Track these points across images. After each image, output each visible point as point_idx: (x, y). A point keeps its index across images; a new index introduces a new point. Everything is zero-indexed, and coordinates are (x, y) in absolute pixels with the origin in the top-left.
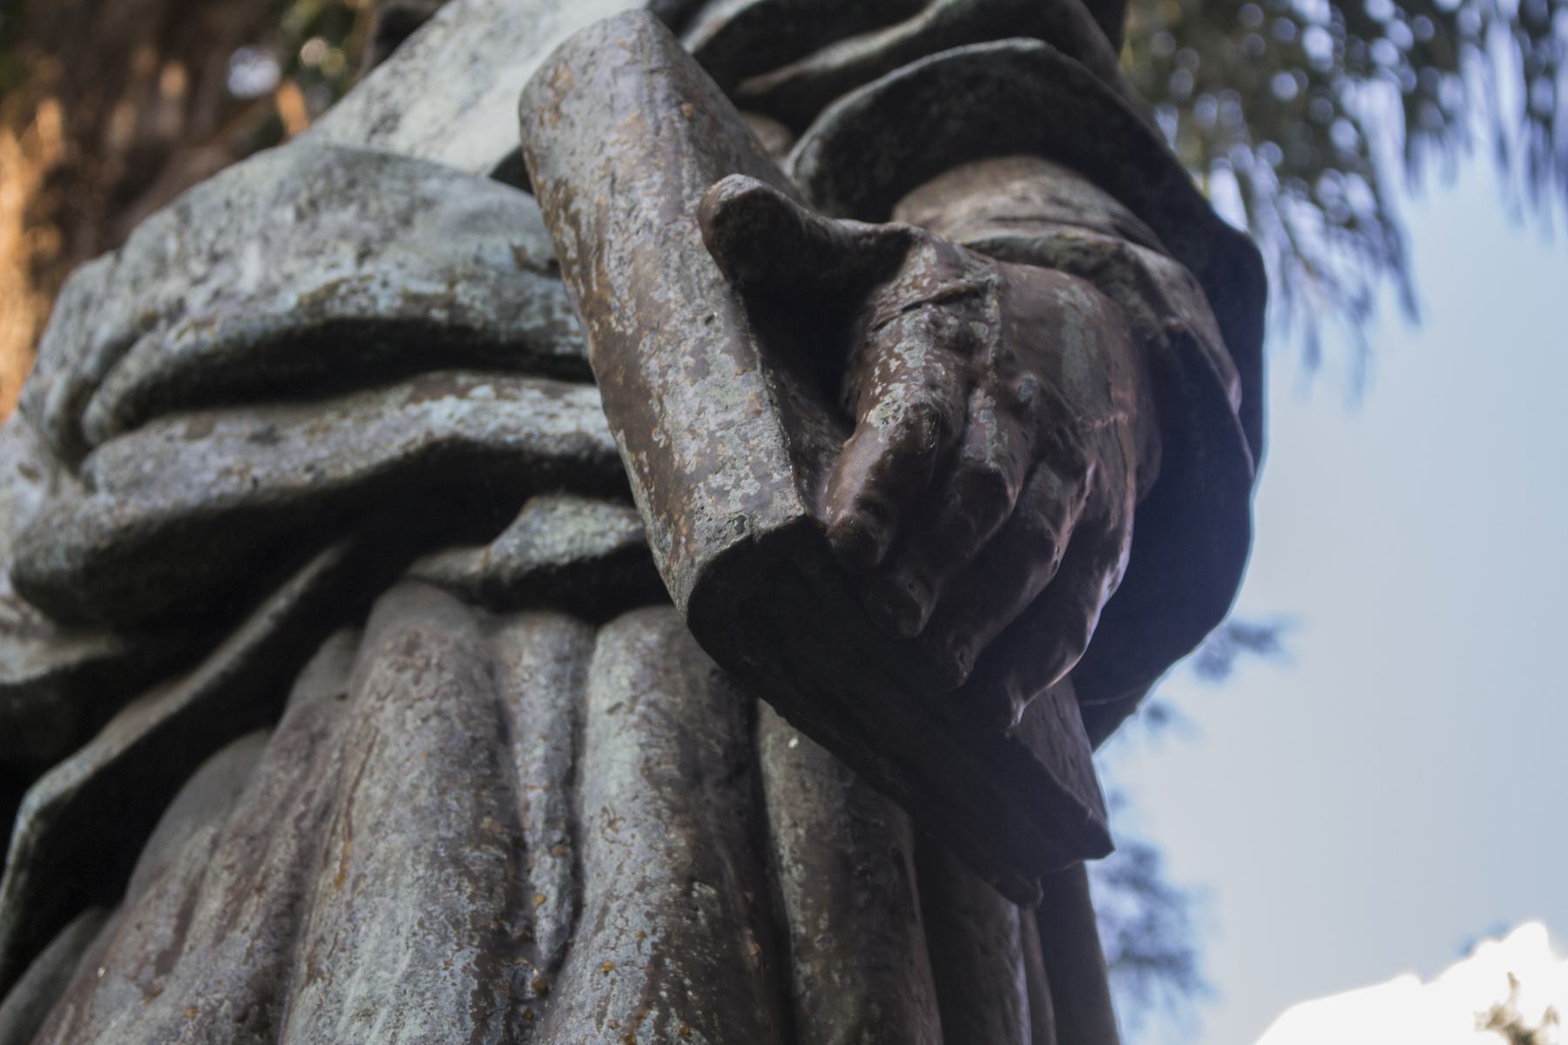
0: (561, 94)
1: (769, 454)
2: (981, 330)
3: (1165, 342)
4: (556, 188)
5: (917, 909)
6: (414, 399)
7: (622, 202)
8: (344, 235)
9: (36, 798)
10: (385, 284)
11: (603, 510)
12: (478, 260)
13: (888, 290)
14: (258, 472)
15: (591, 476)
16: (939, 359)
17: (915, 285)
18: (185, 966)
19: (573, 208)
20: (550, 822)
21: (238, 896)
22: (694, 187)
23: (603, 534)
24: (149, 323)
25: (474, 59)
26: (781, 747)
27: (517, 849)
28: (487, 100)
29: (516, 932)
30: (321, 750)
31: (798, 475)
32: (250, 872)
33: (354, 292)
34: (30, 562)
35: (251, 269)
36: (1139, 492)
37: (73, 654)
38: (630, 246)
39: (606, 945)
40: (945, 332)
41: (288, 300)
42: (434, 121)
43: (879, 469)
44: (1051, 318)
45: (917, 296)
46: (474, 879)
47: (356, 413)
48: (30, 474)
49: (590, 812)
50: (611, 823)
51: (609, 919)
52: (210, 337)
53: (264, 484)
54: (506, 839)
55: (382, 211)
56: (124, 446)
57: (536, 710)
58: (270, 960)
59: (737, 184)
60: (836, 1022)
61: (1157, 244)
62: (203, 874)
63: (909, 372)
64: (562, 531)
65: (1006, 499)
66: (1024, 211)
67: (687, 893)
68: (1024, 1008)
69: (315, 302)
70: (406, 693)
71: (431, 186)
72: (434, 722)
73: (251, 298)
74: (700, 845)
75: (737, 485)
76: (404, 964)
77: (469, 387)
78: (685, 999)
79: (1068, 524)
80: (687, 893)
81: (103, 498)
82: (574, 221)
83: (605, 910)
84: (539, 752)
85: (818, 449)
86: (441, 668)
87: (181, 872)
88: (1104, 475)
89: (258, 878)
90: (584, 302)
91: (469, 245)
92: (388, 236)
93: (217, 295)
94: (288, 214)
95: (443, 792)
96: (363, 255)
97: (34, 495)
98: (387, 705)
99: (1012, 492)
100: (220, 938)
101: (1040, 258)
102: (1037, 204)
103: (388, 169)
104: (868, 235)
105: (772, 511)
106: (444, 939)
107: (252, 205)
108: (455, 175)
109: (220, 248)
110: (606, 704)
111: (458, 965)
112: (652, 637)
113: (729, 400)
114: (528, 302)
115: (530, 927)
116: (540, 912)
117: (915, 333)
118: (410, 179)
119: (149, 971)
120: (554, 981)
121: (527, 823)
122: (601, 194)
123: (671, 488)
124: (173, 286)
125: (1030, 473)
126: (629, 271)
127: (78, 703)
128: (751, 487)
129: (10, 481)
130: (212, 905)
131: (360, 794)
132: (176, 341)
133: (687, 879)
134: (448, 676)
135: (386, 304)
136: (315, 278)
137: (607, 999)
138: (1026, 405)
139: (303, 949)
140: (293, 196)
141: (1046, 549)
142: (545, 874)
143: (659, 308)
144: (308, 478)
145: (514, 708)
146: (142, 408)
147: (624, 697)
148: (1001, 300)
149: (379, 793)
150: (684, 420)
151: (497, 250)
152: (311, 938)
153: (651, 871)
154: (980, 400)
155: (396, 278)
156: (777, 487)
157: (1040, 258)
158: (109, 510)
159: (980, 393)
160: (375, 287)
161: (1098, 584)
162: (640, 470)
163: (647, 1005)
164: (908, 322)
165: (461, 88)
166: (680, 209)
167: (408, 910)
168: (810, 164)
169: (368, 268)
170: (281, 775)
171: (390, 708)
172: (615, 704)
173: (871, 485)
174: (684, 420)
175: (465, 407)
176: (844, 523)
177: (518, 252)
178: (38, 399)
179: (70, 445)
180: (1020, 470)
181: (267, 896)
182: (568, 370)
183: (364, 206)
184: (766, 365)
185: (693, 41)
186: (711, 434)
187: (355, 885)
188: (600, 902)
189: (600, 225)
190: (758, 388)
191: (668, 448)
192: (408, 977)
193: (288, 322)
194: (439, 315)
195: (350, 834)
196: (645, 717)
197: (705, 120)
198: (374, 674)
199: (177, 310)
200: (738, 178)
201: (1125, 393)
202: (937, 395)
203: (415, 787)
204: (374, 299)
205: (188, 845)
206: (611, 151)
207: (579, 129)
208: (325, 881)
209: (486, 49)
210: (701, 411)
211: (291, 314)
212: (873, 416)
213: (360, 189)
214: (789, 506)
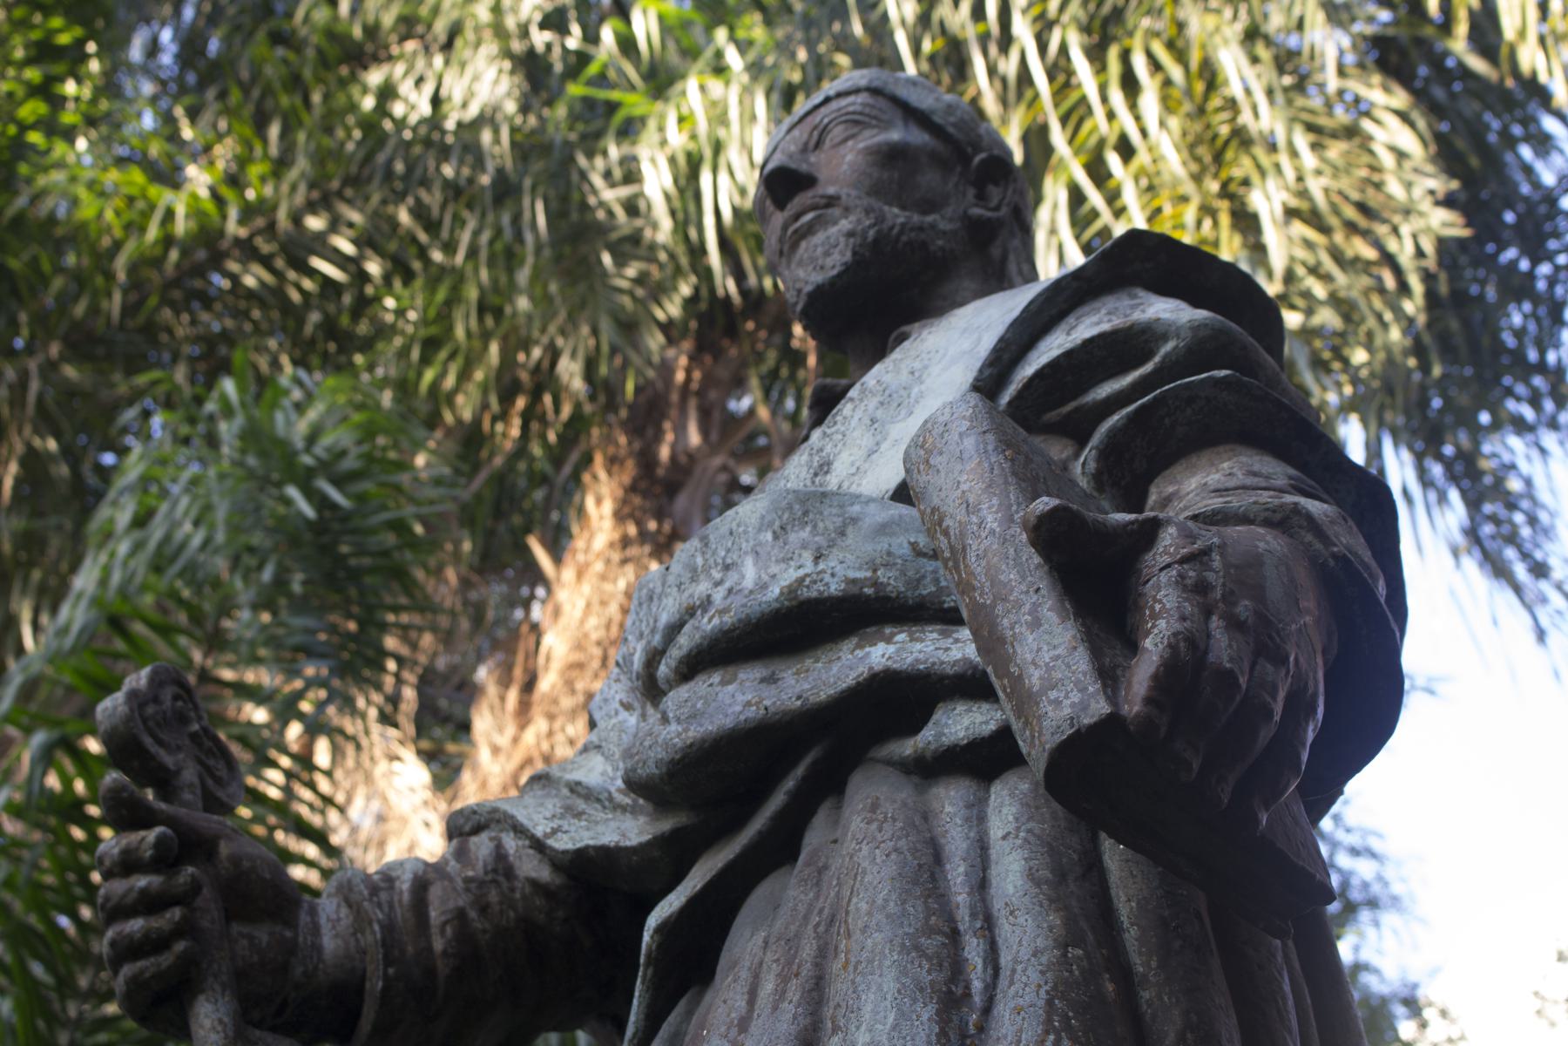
0: (929, 452)
1: (1085, 674)
2: (1211, 576)
3: (1332, 563)
4: (933, 512)
5: (1214, 947)
6: (860, 646)
7: (974, 519)
8: (804, 546)
9: (653, 920)
10: (833, 575)
11: (985, 706)
12: (889, 554)
13: (1149, 556)
14: (767, 703)
15: (971, 685)
16: (1186, 600)
17: (1166, 552)
18: (755, 1027)
19: (944, 525)
20: (973, 915)
21: (784, 979)
22: (1019, 504)
23: (986, 723)
24: (691, 612)
25: (873, 421)
26: (1113, 854)
27: (954, 935)
28: (884, 447)
29: (959, 991)
30: (825, 878)
31: (1105, 686)
32: (790, 963)
33: (815, 582)
34: (634, 770)
35: (750, 573)
36: (1325, 664)
37: (666, 825)
38: (982, 547)
39: (1016, 995)
40: (1188, 582)
41: (775, 591)
42: (852, 464)
43: (1156, 677)
44: (1255, 562)
45: (1167, 559)
46: (929, 959)
47: (824, 659)
48: (627, 707)
49: (997, 905)
50: (1012, 913)
51: (1017, 977)
52: (728, 619)
53: (772, 709)
54: (946, 929)
55: (826, 528)
56: (683, 692)
57: (956, 842)
58: (808, 1020)
59: (1045, 503)
60: (1169, 1027)
61: (1325, 496)
62: (761, 964)
63: (1167, 611)
64: (960, 723)
65: (1239, 686)
66: (1232, 483)
67: (1065, 955)
68: (1291, 1002)
69: (791, 591)
70: (874, 838)
71: (856, 509)
72: (893, 856)
73: (751, 592)
74: (1070, 922)
75: (1067, 697)
76: (891, 1020)
77: (893, 635)
78: (1070, 1025)
79: (1282, 695)
80: (1065, 955)
81: (674, 727)
82: (946, 533)
83: (1014, 971)
84: (961, 869)
85: (1116, 666)
86: (894, 820)
87: (747, 964)
88: (1301, 660)
89: (795, 967)
90: (958, 585)
91: (883, 544)
92: (832, 544)
93: (730, 591)
94: (769, 536)
95: (904, 902)
96: (817, 559)
97: (632, 720)
98: (862, 843)
99: (1243, 681)
100: (775, 1008)
101: (1244, 519)
102: (1240, 478)
103: (827, 501)
104: (1132, 523)
105: (1090, 712)
106: (915, 1001)
107: (745, 532)
108: (870, 500)
109: (729, 561)
110: (1000, 834)
111: (925, 1017)
112: (1025, 786)
113: (1056, 642)
114: (924, 577)
115: (968, 987)
116: (973, 976)
117: (1168, 584)
118: (841, 506)
119: (734, 1032)
120: (987, 1021)
121: (959, 918)
122: (961, 515)
123: (1024, 701)
124: (702, 588)
125: (1252, 669)
126: (984, 563)
127: (671, 857)
128: (1076, 697)
129: (617, 713)
130: (768, 986)
131: (852, 908)
132: (708, 624)
133: (1064, 946)
134: (899, 825)
135: (835, 588)
136: (790, 575)
137: (1021, 1031)
138: (1245, 622)
139: (828, 1012)
140: (770, 524)
141: (1269, 713)
142: (973, 951)
143: (1005, 585)
144: (799, 703)
145: (943, 841)
146: (692, 667)
147: (1011, 828)
148: (1222, 555)
149: (864, 906)
150: (1029, 657)
151: (900, 545)
152: (832, 1004)
153: (1040, 942)
154: (1215, 622)
155: (839, 570)
156: (1093, 695)
157: (1244, 519)
158: (679, 735)
159: (1214, 618)
160: (827, 578)
161: (1305, 731)
162: (1004, 691)
163: (1047, 1032)
164: (1164, 577)
165: (867, 441)
166: (1012, 521)
167: (890, 984)
168: (1092, 465)
169: (821, 566)
170: (802, 897)
171: (865, 848)
172: (1005, 830)
173: (1151, 688)
174: (1029, 657)
175: (891, 649)
176: (1137, 715)
177: (914, 545)
178: (628, 659)
179: (651, 689)
180: (1246, 666)
181: (801, 980)
182: (950, 618)
183: (815, 526)
184: (1077, 615)
185: (1005, 398)
186: (1047, 665)
187: (856, 968)
188: (1010, 965)
189: (962, 534)
190: (1072, 632)
191: (1020, 675)
192: (895, 1027)
193: (776, 605)
194: (868, 591)
195: (849, 936)
196: (1025, 839)
197: (1021, 458)
198: (853, 827)
199: (707, 602)
200: (1045, 499)
201: (1309, 602)
202: (1188, 624)
203: (886, 901)
204: (827, 584)
205: (747, 944)
206: (964, 487)
207: (943, 474)
208: (836, 966)
209: (879, 414)
210: (1039, 650)
211: (777, 600)
212: (1148, 643)
213: (811, 516)
214: (1101, 708)
